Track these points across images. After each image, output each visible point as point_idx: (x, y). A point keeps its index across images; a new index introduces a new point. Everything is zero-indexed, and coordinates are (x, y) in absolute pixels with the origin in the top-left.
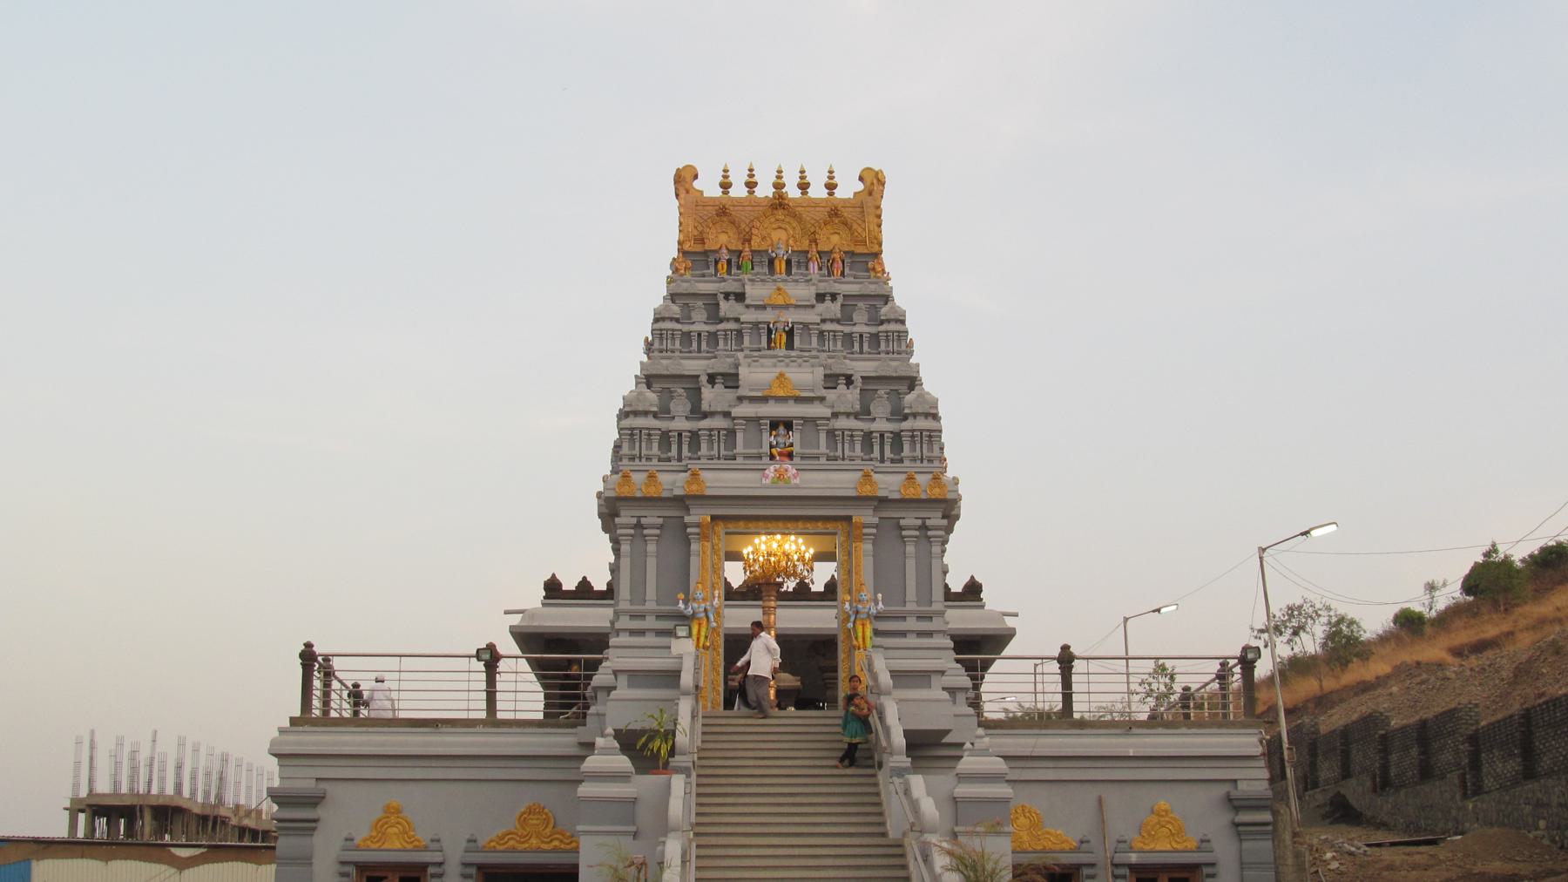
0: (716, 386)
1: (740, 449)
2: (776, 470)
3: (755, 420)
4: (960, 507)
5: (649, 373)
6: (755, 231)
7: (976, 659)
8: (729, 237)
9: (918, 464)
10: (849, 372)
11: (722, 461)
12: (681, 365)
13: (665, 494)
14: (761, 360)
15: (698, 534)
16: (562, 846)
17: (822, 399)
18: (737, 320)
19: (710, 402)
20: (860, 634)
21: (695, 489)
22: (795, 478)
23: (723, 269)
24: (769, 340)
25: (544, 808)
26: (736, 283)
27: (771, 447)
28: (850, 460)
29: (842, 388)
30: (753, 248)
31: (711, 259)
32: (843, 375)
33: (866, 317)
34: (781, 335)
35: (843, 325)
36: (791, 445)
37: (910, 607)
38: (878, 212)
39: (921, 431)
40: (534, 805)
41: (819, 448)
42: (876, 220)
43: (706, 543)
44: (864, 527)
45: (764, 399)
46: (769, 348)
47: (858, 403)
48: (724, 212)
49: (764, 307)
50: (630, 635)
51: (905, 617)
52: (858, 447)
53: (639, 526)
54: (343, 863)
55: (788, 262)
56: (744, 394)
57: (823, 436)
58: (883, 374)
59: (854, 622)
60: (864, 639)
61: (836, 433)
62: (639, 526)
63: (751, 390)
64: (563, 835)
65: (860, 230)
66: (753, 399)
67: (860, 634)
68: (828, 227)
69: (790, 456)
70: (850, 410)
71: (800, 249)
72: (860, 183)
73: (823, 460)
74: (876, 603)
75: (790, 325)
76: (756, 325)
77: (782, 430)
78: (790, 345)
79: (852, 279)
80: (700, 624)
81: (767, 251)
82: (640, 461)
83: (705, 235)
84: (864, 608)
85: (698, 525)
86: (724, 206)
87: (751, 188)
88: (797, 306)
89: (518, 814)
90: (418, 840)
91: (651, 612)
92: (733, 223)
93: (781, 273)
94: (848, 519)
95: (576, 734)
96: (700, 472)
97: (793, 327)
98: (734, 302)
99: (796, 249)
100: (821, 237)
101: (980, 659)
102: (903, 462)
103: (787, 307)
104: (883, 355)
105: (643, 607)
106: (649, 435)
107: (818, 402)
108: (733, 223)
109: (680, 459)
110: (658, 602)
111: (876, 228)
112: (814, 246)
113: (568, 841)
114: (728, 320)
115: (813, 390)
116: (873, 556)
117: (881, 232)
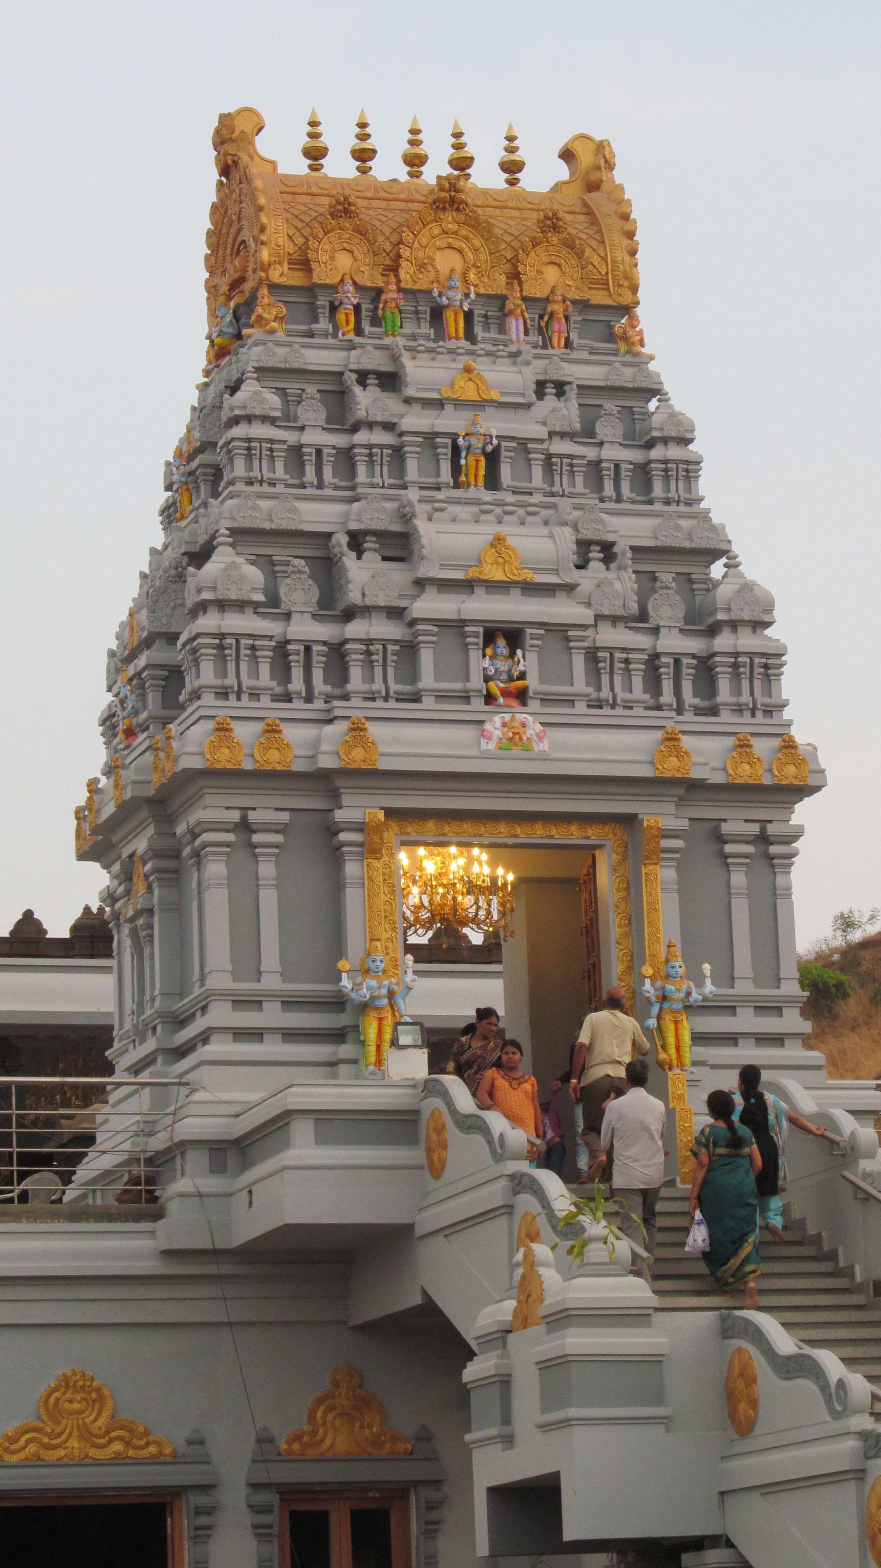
0: (366, 555)
1: (427, 680)
2: (504, 725)
3: (457, 626)
4: (801, 800)
5: (235, 525)
6: (405, 252)
7: (10, 1083)
8: (355, 260)
9: (747, 718)
10: (610, 538)
11: (392, 704)
12: (294, 510)
13: (298, 766)
14: (452, 509)
15: (361, 845)
16: (131, 1453)
17: (570, 588)
18: (389, 427)
19: (363, 589)
20: (671, 1041)
21: (358, 758)
22: (541, 739)
23: (348, 323)
24: (456, 470)
25: (92, 1379)
26: (378, 353)
27: (487, 679)
28: (625, 707)
29: (596, 566)
30: (525, 294)
31: (322, 301)
32: (597, 543)
33: (323, 415)
34: (477, 461)
35: (280, 427)
36: (522, 676)
37: (744, 988)
38: (628, 227)
39: (237, 637)
40: (74, 1373)
41: (572, 685)
42: (625, 242)
43: (375, 863)
44: (665, 837)
45: (467, 586)
46: (457, 485)
47: (636, 598)
48: (346, 211)
49: (439, 404)
50: (757, 1045)
51: (734, 1007)
52: (265, 669)
53: (245, 827)
54: (255, 1486)
55: (469, 316)
56: (431, 574)
57: (579, 661)
58: (669, 543)
59: (659, 1018)
60: (678, 1048)
61: (600, 654)
62: (245, 827)
63: (443, 566)
64: (131, 1431)
65: (596, 260)
66: (445, 585)
67: (671, 1041)
68: (540, 250)
69: (522, 696)
70: (620, 612)
71: (491, 292)
72: (562, 164)
73: (581, 707)
74: (700, 984)
75: (495, 442)
76: (430, 438)
77: (502, 645)
78: (492, 482)
79: (585, 355)
80: (380, 1020)
81: (430, 292)
82: (239, 699)
83: (311, 255)
84: (678, 990)
85: (360, 827)
86: (346, 199)
87: (364, 161)
88: (501, 405)
89: (42, 1390)
90: (158, 1443)
91: (273, 995)
92: (361, 231)
93: (457, 338)
94: (629, 821)
95: (153, 1232)
96: (368, 725)
97: (499, 445)
98: (378, 389)
99: (482, 291)
100: (527, 271)
101: (17, 1084)
102: (469, 703)
103: (481, 404)
104: (658, 507)
105: (254, 986)
106: (627, 661)
107: (564, 594)
108: (361, 231)
109: (309, 698)
110: (285, 976)
111: (628, 259)
112: (517, 287)
113: (142, 1442)
114: (370, 425)
115: (556, 571)
116: (679, 892)
117: (636, 265)
